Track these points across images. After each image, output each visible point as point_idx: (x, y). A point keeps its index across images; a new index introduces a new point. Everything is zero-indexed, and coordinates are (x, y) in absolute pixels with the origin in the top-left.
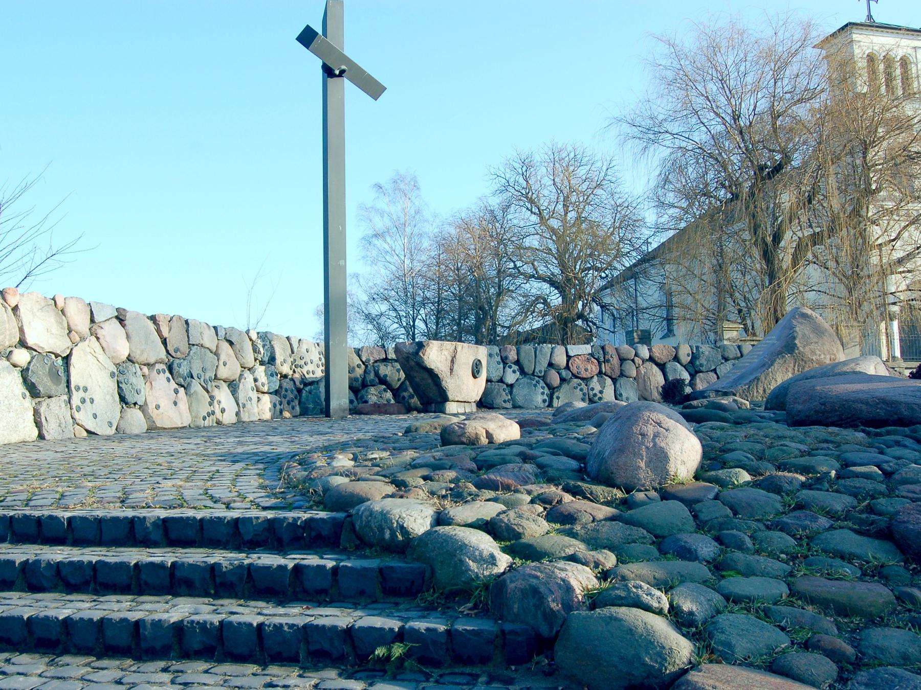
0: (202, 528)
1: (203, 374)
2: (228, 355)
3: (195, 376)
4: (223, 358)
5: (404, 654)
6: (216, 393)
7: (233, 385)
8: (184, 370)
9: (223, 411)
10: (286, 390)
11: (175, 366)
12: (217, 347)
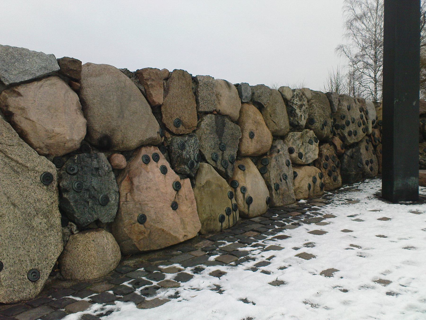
0: (271, 94)
2: (257, 123)
3: (208, 156)
4: (249, 126)
6: (239, 176)
7: (261, 160)
8: (190, 152)
9: (249, 201)
10: (327, 158)
11: (175, 147)
12: (241, 112)
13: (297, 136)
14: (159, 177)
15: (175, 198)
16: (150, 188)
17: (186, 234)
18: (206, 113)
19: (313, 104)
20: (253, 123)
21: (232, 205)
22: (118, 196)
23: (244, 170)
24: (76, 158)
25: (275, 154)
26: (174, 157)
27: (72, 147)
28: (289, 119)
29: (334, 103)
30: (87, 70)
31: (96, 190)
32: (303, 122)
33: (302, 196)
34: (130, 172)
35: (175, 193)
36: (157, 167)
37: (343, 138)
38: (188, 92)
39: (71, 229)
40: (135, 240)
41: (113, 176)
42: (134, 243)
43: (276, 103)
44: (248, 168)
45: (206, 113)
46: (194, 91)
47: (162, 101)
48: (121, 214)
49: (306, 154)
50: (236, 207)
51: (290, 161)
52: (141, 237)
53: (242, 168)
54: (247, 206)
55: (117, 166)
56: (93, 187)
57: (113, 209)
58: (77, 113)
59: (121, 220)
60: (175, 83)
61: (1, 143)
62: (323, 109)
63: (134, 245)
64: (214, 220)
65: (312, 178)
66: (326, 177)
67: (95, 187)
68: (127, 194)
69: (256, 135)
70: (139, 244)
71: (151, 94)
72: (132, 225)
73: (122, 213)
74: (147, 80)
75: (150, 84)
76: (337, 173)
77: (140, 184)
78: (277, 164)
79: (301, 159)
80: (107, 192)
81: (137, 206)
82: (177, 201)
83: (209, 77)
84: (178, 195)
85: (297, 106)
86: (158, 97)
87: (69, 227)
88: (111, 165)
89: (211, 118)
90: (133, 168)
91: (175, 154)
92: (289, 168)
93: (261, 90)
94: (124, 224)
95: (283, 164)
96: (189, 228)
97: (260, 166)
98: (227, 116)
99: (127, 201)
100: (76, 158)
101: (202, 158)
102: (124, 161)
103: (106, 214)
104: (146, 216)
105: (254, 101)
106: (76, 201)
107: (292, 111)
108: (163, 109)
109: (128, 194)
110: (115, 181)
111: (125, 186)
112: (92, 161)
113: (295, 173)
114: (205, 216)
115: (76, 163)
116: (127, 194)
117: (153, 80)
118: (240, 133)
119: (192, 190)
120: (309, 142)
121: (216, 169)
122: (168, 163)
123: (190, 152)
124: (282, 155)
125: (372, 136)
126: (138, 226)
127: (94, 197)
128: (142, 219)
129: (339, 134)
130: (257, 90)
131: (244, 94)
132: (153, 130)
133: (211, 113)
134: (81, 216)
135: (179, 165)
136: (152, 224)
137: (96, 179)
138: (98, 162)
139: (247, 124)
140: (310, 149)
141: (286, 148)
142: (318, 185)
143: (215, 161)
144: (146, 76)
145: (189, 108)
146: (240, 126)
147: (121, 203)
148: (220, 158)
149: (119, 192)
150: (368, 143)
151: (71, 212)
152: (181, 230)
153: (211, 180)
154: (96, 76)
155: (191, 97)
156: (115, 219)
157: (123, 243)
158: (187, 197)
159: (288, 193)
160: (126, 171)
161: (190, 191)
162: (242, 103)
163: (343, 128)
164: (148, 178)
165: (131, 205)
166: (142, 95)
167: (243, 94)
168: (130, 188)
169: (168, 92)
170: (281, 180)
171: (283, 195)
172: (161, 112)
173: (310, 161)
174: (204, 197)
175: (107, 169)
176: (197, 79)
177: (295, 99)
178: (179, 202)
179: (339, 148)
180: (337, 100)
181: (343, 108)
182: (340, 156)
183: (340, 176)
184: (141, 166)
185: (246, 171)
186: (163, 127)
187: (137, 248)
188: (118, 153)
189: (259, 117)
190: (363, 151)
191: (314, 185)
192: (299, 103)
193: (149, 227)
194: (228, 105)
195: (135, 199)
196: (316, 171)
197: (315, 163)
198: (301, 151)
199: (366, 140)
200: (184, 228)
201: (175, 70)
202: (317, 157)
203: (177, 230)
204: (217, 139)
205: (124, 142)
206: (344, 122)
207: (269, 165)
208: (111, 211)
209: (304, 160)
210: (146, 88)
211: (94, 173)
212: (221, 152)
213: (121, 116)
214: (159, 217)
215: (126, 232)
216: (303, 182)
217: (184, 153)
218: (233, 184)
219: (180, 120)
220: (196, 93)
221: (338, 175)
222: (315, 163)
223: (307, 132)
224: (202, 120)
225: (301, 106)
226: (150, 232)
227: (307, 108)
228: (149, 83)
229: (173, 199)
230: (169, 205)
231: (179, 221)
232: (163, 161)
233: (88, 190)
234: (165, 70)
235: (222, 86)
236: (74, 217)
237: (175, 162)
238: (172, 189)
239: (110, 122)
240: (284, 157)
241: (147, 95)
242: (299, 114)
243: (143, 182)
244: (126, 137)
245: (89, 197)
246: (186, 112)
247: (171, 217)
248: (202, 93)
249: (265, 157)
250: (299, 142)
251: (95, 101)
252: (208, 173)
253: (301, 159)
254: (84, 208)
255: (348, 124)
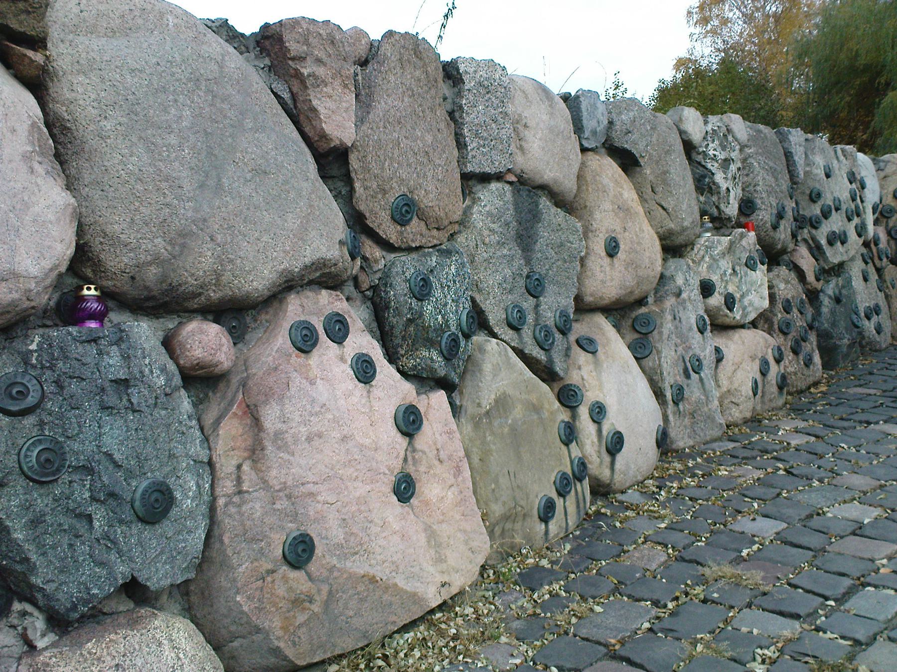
1: (528, 304)
2: (623, 209)
3: (495, 316)
4: (605, 221)
5: (675, 86)
6: (582, 371)
9: (615, 445)
11: (399, 291)
12: (580, 177)
13: (720, 248)
14: (348, 395)
15: (405, 460)
16: (320, 436)
17: (446, 579)
18: (485, 178)
19: (751, 160)
20: (613, 211)
21: (572, 462)
22: (207, 478)
23: (594, 353)
24: (33, 347)
25: (670, 302)
26: (396, 322)
27: (13, 304)
28: (643, 207)
29: (796, 158)
30: (76, 10)
31: (118, 466)
32: (732, 209)
33: (737, 415)
34: (250, 383)
35: (402, 442)
36: (342, 359)
37: (816, 251)
38: (432, 110)
39: (25, 629)
40: (280, 633)
41: (185, 404)
42: (276, 643)
43: (668, 152)
44: (604, 347)
45: (485, 178)
46: (449, 107)
47: (353, 137)
48: (222, 542)
49: (743, 296)
50: (581, 469)
51: (706, 317)
52: (301, 618)
53: (587, 345)
54: (607, 459)
55: (202, 368)
56: (109, 456)
57: (190, 532)
58: (32, 171)
59: (225, 564)
60: (392, 78)
61: (3, 280)
62: (773, 172)
63: (276, 652)
64: (525, 515)
65: (757, 362)
66: (789, 356)
67: (117, 456)
68: (239, 467)
69: (622, 246)
70: (294, 644)
71: (314, 110)
72: (263, 579)
73: (226, 540)
74: (301, 59)
75: (309, 75)
76: (811, 344)
77: (284, 427)
78: (676, 328)
79: (731, 310)
80: (167, 469)
81: (278, 506)
82: (411, 469)
83: (491, 64)
84: (414, 451)
85: (716, 165)
86: (338, 119)
87: (16, 622)
88: (178, 365)
89: (501, 196)
90: (257, 370)
91: (398, 312)
92: (704, 339)
93: (631, 114)
94: (235, 580)
95: (690, 329)
96: (453, 558)
97: (632, 336)
98: (544, 188)
99: (240, 492)
100: (33, 347)
101: (479, 321)
102: (225, 349)
103: (162, 553)
104: (311, 539)
105: (612, 145)
106: (36, 522)
107: (704, 177)
108: (354, 162)
109: (246, 468)
110: (194, 422)
111: (234, 438)
112: (100, 353)
113: (717, 350)
114: (497, 510)
115: (34, 367)
116: (239, 467)
117: (319, 61)
118: (581, 240)
119: (455, 427)
120: (746, 265)
121: (520, 353)
122: (375, 343)
123: (446, 305)
124: (688, 304)
125: (872, 245)
126: (285, 579)
127: (112, 495)
128: (300, 551)
129: (805, 240)
130: (620, 113)
131: (589, 124)
132: (324, 237)
133: (499, 177)
134: (62, 578)
135: (414, 348)
136: (334, 561)
137: (120, 422)
138: (126, 358)
139: (598, 215)
140: (752, 283)
141: (695, 283)
142: (774, 382)
143: (515, 329)
144: (294, 47)
145: (438, 162)
146: (580, 218)
147: (221, 502)
148: (530, 319)
149: (210, 464)
150: (866, 263)
151: (18, 568)
152: (431, 569)
153: (510, 391)
154: (112, 33)
155: (442, 125)
156: (199, 568)
157: (236, 644)
158: (443, 455)
159: (706, 409)
160: (235, 380)
161: (450, 433)
162: (584, 150)
163: (814, 224)
164: (313, 401)
165: (257, 506)
166: (285, 115)
167: (585, 122)
168: (249, 442)
169: (369, 106)
170: (688, 376)
171: (692, 415)
172: (349, 172)
173: (752, 316)
174: (493, 447)
175: (162, 381)
176: (458, 70)
177: (711, 145)
178: (418, 472)
179: (811, 278)
180: (802, 149)
181: (815, 171)
182: (813, 296)
183: (817, 352)
184: (289, 363)
185: (600, 353)
186: (358, 223)
187: (285, 658)
188: (206, 319)
189: (629, 194)
190: (857, 283)
191: (763, 381)
192: (721, 156)
193: (325, 573)
194: (547, 154)
195: (273, 482)
196: (766, 341)
197: (762, 321)
198: (731, 289)
199: (862, 255)
200: (440, 560)
201: (390, 34)
202: (766, 304)
203: (416, 570)
204: (519, 262)
205: (224, 279)
206: (816, 210)
207: (655, 332)
208: (185, 540)
209: (737, 314)
210: (295, 90)
211: (111, 399)
212: (532, 301)
213: (211, 183)
214: (356, 535)
215: (245, 608)
216: (740, 375)
217: (428, 308)
218: (568, 397)
219: (412, 200)
220: (454, 115)
221: (813, 350)
222: (762, 321)
223: (742, 236)
224: (474, 201)
225: (726, 163)
226: (330, 592)
227: (739, 169)
228: (305, 72)
229: (397, 465)
230: (388, 489)
231: (422, 539)
232: (362, 341)
233: (87, 469)
234: (359, 34)
235: (526, 97)
236: (32, 587)
237: (398, 341)
238: (394, 431)
239: (167, 205)
240: (693, 310)
241: (298, 114)
242: (724, 185)
243: (298, 419)
244: (231, 261)
245: (93, 499)
246: (429, 175)
247: (396, 526)
248: (475, 114)
249: (643, 310)
250: (725, 265)
251: (108, 125)
252: (498, 370)
253: (731, 310)
254: (71, 546)
255: (826, 214)
